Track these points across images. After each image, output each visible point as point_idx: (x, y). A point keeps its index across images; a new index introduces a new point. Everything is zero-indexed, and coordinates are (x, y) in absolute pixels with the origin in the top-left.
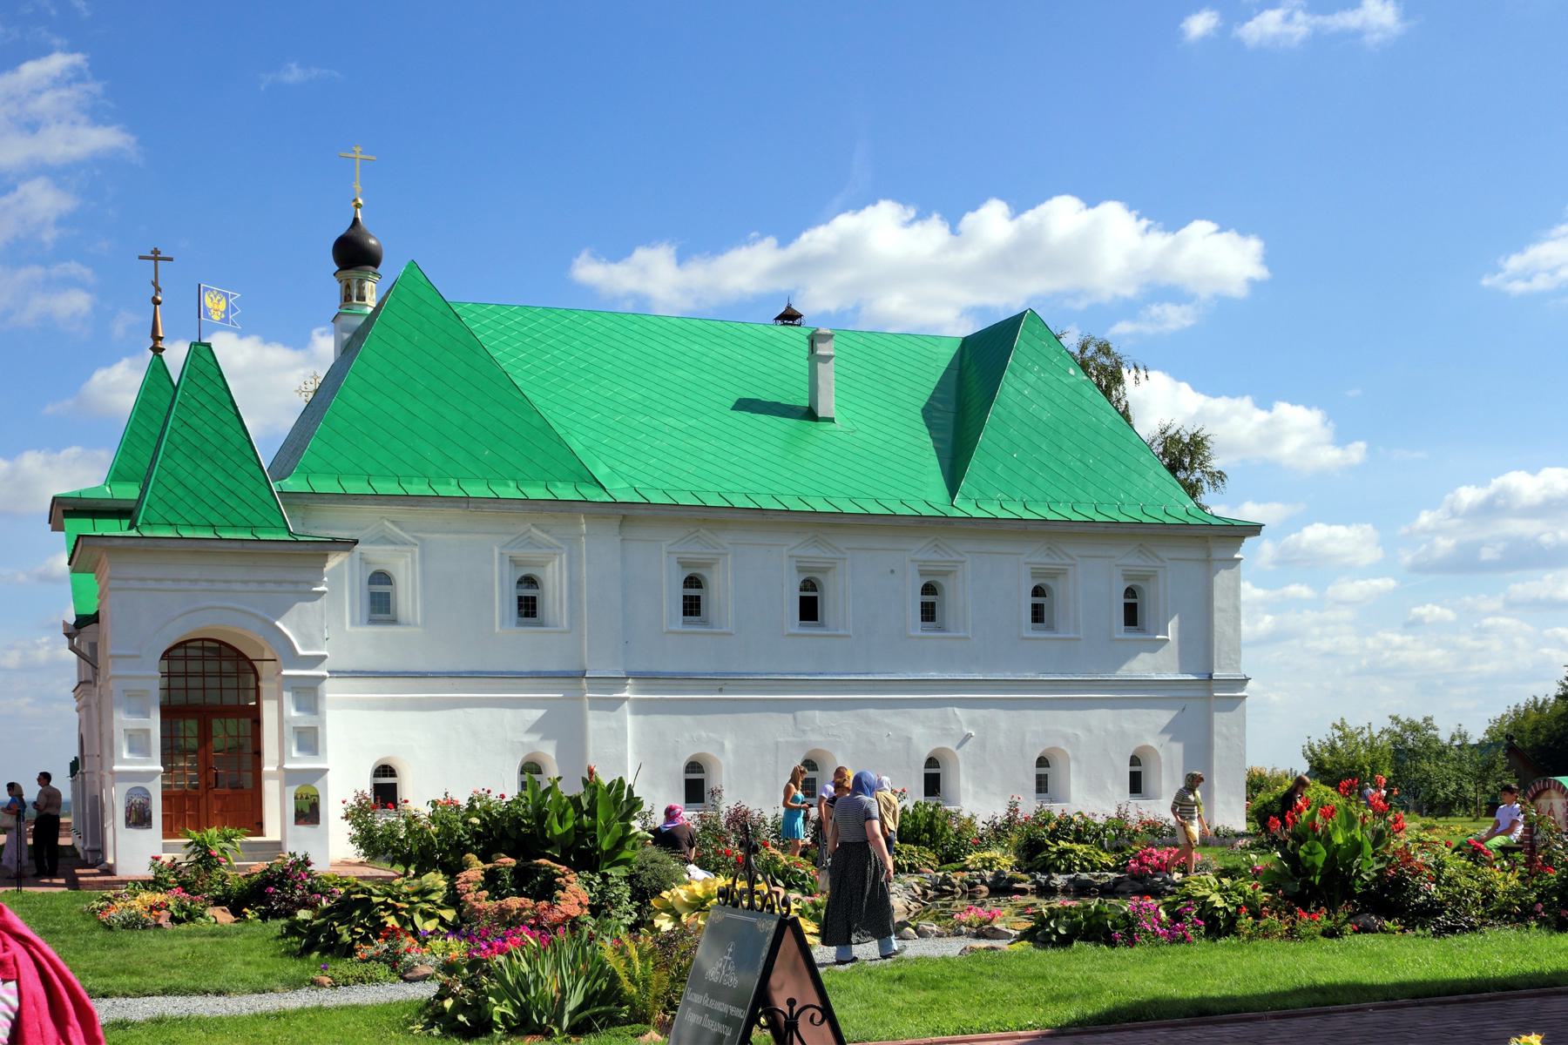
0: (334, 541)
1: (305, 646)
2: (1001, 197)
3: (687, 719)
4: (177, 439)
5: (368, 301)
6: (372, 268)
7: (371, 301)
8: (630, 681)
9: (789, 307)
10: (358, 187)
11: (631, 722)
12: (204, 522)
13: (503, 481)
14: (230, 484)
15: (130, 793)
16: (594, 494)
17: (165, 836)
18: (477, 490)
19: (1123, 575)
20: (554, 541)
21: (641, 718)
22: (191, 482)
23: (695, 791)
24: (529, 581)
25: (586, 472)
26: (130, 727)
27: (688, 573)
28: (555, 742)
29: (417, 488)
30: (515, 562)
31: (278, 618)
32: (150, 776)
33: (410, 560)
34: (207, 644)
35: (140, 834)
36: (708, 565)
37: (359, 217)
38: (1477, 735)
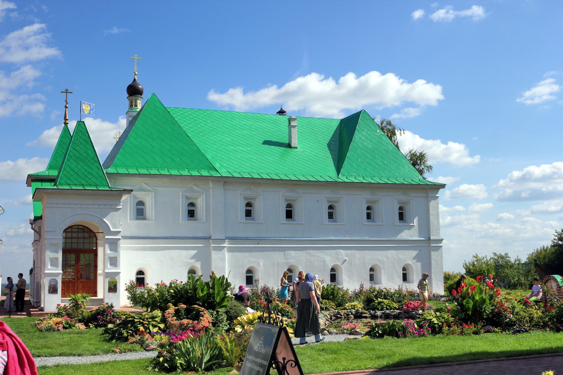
0: (125, 190)
1: (113, 228)
2: (353, 72)
3: (247, 254)
4: (72, 154)
5: (138, 107)
6: (140, 96)
7: (139, 107)
8: (227, 240)
9: (281, 109)
10: (136, 69)
11: (227, 255)
13: (183, 169)
14: (89, 170)
15: (51, 281)
16: (214, 174)
17: (62, 297)
18: (174, 172)
19: (398, 202)
21: (230, 253)
22: (76, 169)
23: (250, 280)
29: (154, 172)
30: (187, 198)
31: (104, 218)
32: (57, 275)
33: (150, 197)
34: (79, 227)
35: (54, 296)
37: (136, 78)
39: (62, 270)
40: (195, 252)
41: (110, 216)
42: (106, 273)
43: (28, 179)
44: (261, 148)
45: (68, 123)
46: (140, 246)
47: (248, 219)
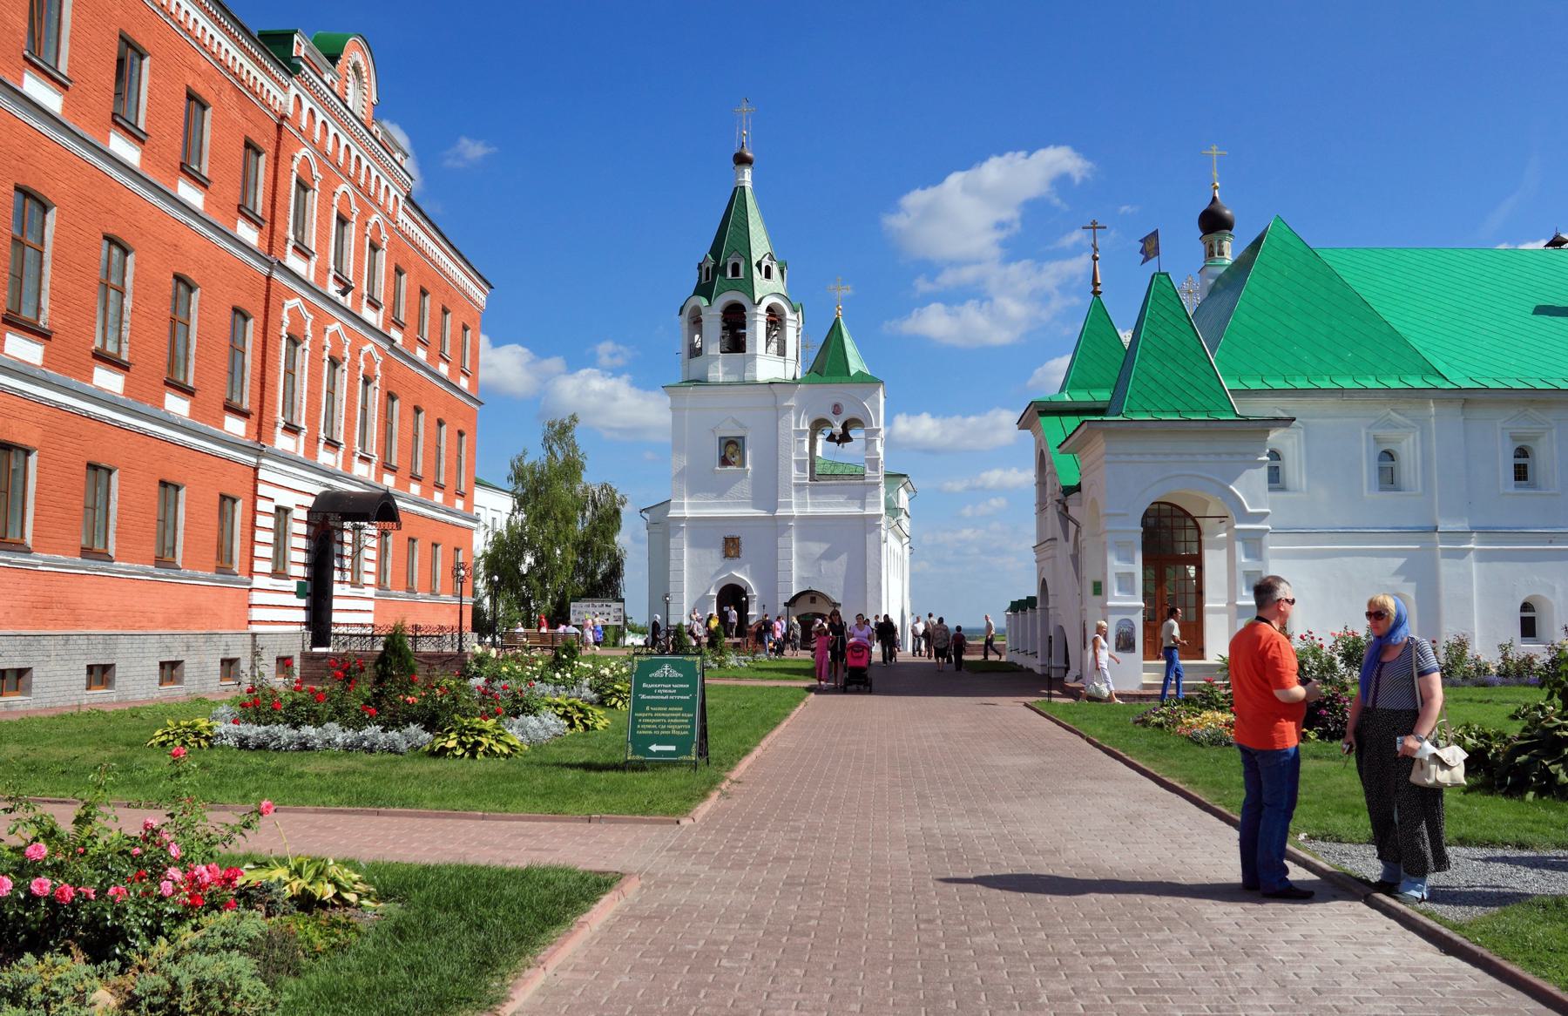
0: (1276, 419)
1: (1252, 506)
2: (900, 412)
4: (1149, 346)
5: (1226, 256)
6: (1227, 231)
7: (1228, 259)
8: (1474, 535)
10: (1216, 174)
11: (1475, 567)
12: (1171, 408)
13: (1365, 376)
14: (1189, 378)
15: (1120, 623)
18: (1348, 383)
20: (1409, 422)
21: (1484, 565)
22: (1159, 377)
23: (1528, 628)
24: (1389, 455)
25: (1429, 366)
26: (1120, 571)
27: (1519, 444)
28: (1414, 584)
29: (1301, 384)
30: (1377, 440)
31: (1231, 482)
32: (1134, 610)
33: (1296, 440)
36: (1535, 438)
37: (1217, 195)
38: (1226, 654)
39: (1144, 601)
40: (1402, 561)
41: (1242, 478)
42: (1239, 607)
43: (1027, 414)
44: (1534, 324)
45: (1100, 292)
46: (691, 565)
47: (1521, 486)
